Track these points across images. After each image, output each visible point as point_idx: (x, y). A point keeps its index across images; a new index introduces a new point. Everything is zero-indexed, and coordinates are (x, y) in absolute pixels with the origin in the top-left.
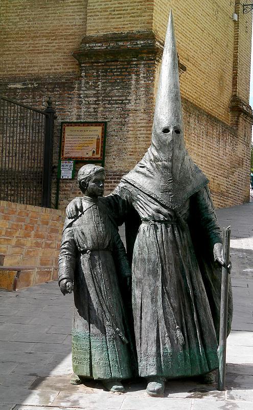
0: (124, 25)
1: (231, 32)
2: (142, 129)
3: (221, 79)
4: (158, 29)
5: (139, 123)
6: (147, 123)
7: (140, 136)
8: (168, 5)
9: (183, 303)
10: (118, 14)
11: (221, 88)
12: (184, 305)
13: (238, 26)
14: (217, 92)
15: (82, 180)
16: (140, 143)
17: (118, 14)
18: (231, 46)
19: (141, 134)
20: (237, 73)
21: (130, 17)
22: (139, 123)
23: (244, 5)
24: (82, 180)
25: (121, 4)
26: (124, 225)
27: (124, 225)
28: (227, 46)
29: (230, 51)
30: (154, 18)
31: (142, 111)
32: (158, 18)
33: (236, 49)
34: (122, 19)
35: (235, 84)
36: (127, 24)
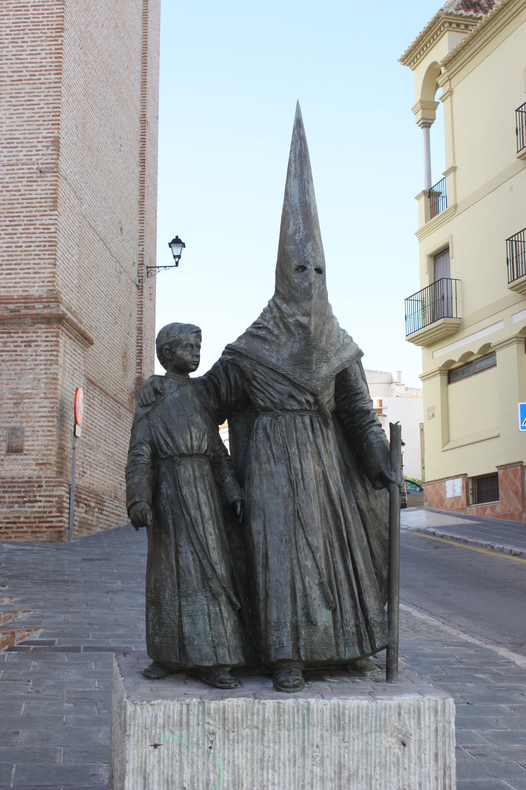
0: (15, 283)
1: (135, 299)
2: (43, 419)
3: (125, 356)
4: (60, 290)
5: (37, 412)
6: (49, 412)
7: (39, 429)
8: (71, 261)
9: (330, 542)
10: (8, 269)
11: (125, 368)
12: (332, 546)
13: (142, 292)
14: (121, 373)
15: (164, 345)
16: (39, 438)
17: (8, 269)
18: (135, 316)
19: (40, 426)
20: (142, 350)
21: (24, 273)
22: (37, 412)
23: (148, 268)
24: (164, 345)
25: (12, 256)
26: (226, 421)
27: (226, 421)
28: (131, 316)
29: (134, 323)
30: (56, 276)
31: (42, 395)
32: (60, 276)
33: (140, 319)
34: (13, 276)
35: (140, 364)
36: (20, 283)
